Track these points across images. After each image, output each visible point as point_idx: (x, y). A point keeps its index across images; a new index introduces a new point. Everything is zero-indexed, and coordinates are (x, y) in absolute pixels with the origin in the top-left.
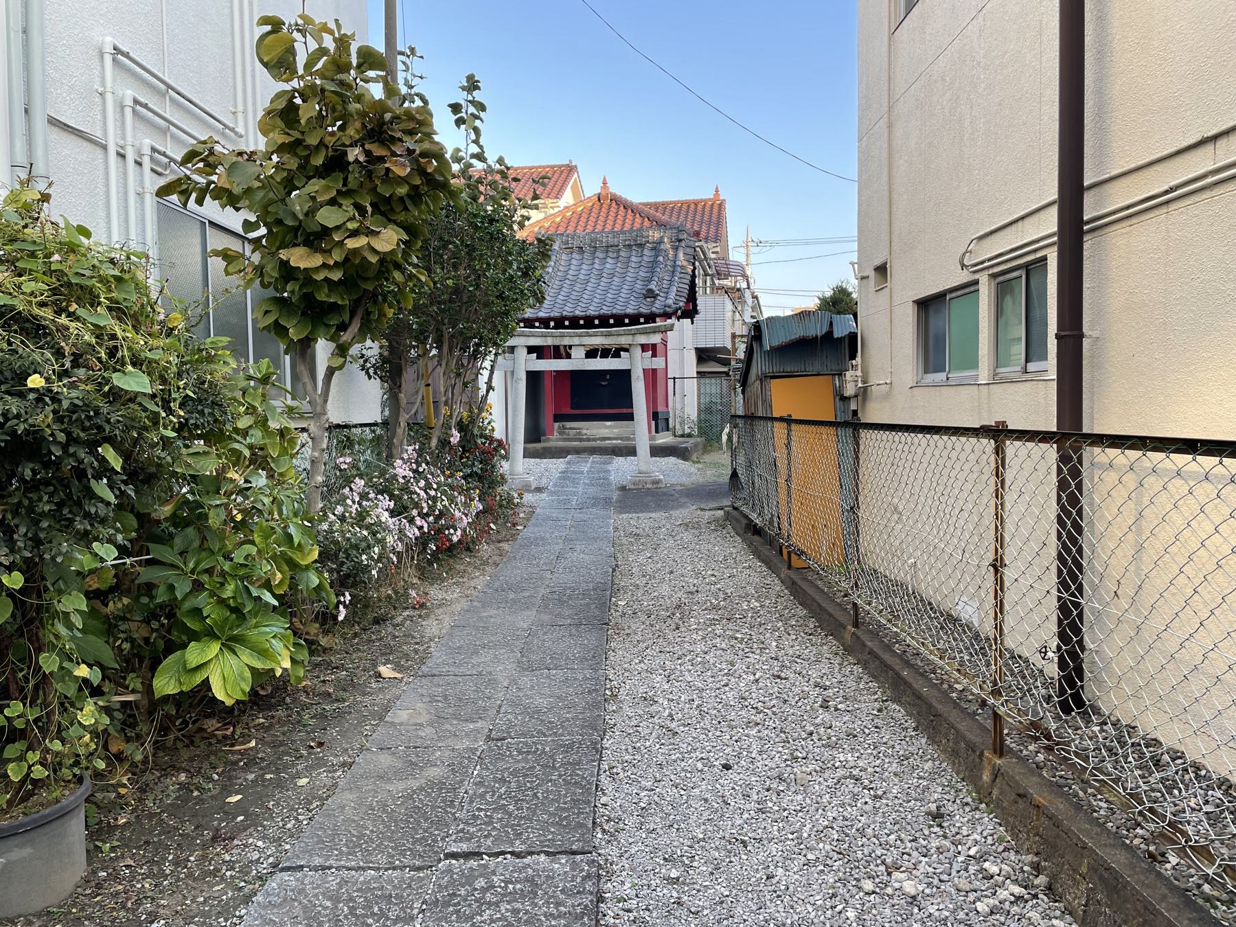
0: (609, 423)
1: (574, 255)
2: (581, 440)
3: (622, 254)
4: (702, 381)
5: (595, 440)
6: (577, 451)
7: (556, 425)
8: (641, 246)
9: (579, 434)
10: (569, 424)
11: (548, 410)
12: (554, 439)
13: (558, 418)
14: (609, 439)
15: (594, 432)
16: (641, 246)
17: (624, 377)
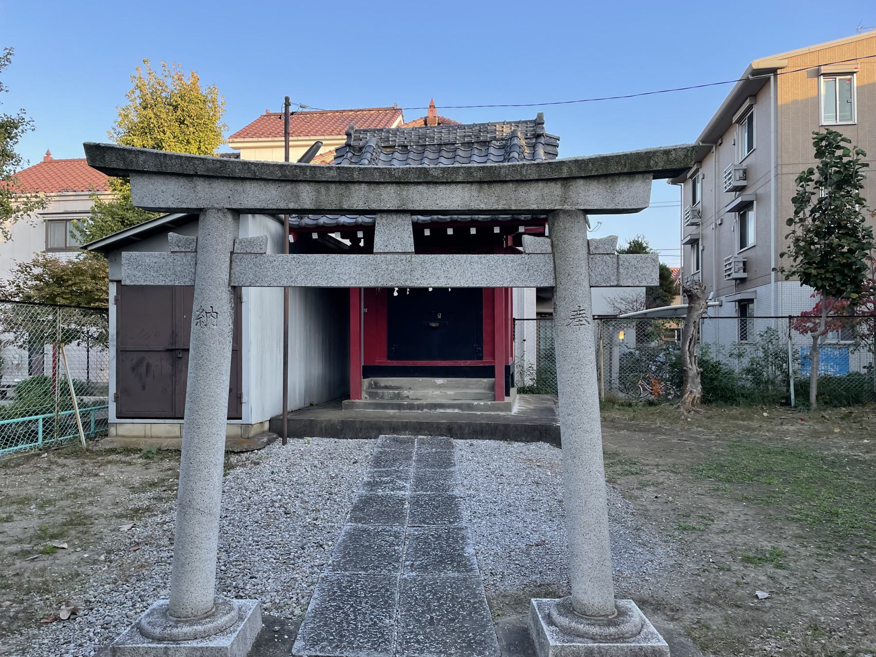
0: (440, 381)
1: (396, 155)
2: (399, 407)
3: (460, 153)
4: (542, 323)
5: (420, 407)
6: (394, 428)
7: (366, 382)
8: (486, 143)
9: (398, 396)
10: (384, 381)
11: (357, 360)
12: (362, 405)
13: (369, 371)
14: (442, 406)
15: (420, 393)
16: (486, 143)
17: (173, 409)
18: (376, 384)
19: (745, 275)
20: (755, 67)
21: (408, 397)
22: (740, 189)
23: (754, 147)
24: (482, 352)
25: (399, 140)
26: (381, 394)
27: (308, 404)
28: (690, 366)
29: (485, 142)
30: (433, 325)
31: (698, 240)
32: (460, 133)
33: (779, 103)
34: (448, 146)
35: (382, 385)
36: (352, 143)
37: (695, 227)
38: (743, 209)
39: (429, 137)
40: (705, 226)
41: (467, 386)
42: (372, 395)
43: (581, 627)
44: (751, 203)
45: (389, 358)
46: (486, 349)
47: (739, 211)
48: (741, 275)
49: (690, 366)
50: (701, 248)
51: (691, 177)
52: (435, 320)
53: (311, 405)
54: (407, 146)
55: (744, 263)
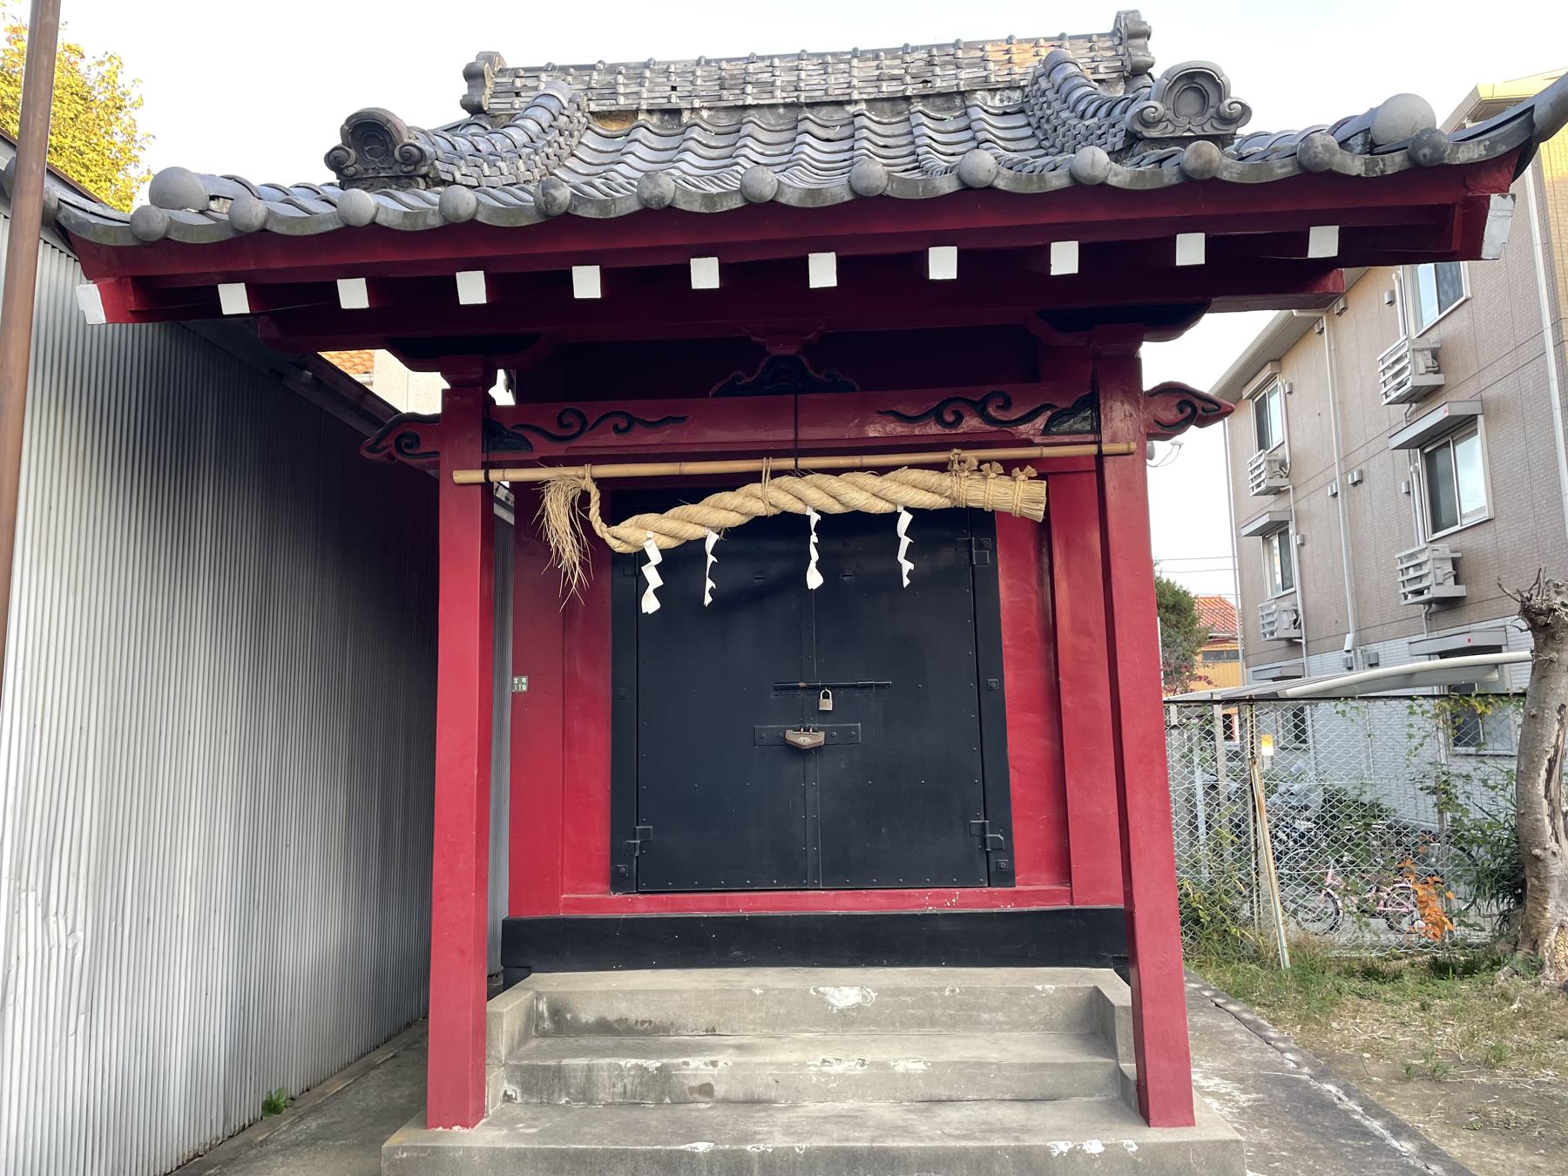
0: (847, 987)
8: (956, 98)
18: (557, 1012)
19: (1458, 591)
20: (1486, 94)
21: (706, 1090)
22: (1421, 396)
23: (1467, 293)
24: (1009, 851)
25: (652, 94)
26: (579, 1079)
27: (250, 1107)
28: (1552, 845)
29: (947, 96)
30: (804, 740)
31: (1286, 523)
32: (863, 70)
33: (1547, 176)
34: (824, 112)
35: (588, 1016)
36: (487, 102)
37: (1271, 498)
38: (1435, 446)
39: (756, 84)
40: (1301, 492)
41: (964, 1017)
42: (539, 1083)
43: (845, 1106)
44: (1472, 419)
45: (618, 882)
46: (1029, 834)
47: (1421, 447)
48: (1450, 590)
49: (1552, 845)
50: (1294, 540)
51: (1251, 397)
52: (808, 717)
53: (271, 1108)
54: (677, 112)
55: (1455, 563)
